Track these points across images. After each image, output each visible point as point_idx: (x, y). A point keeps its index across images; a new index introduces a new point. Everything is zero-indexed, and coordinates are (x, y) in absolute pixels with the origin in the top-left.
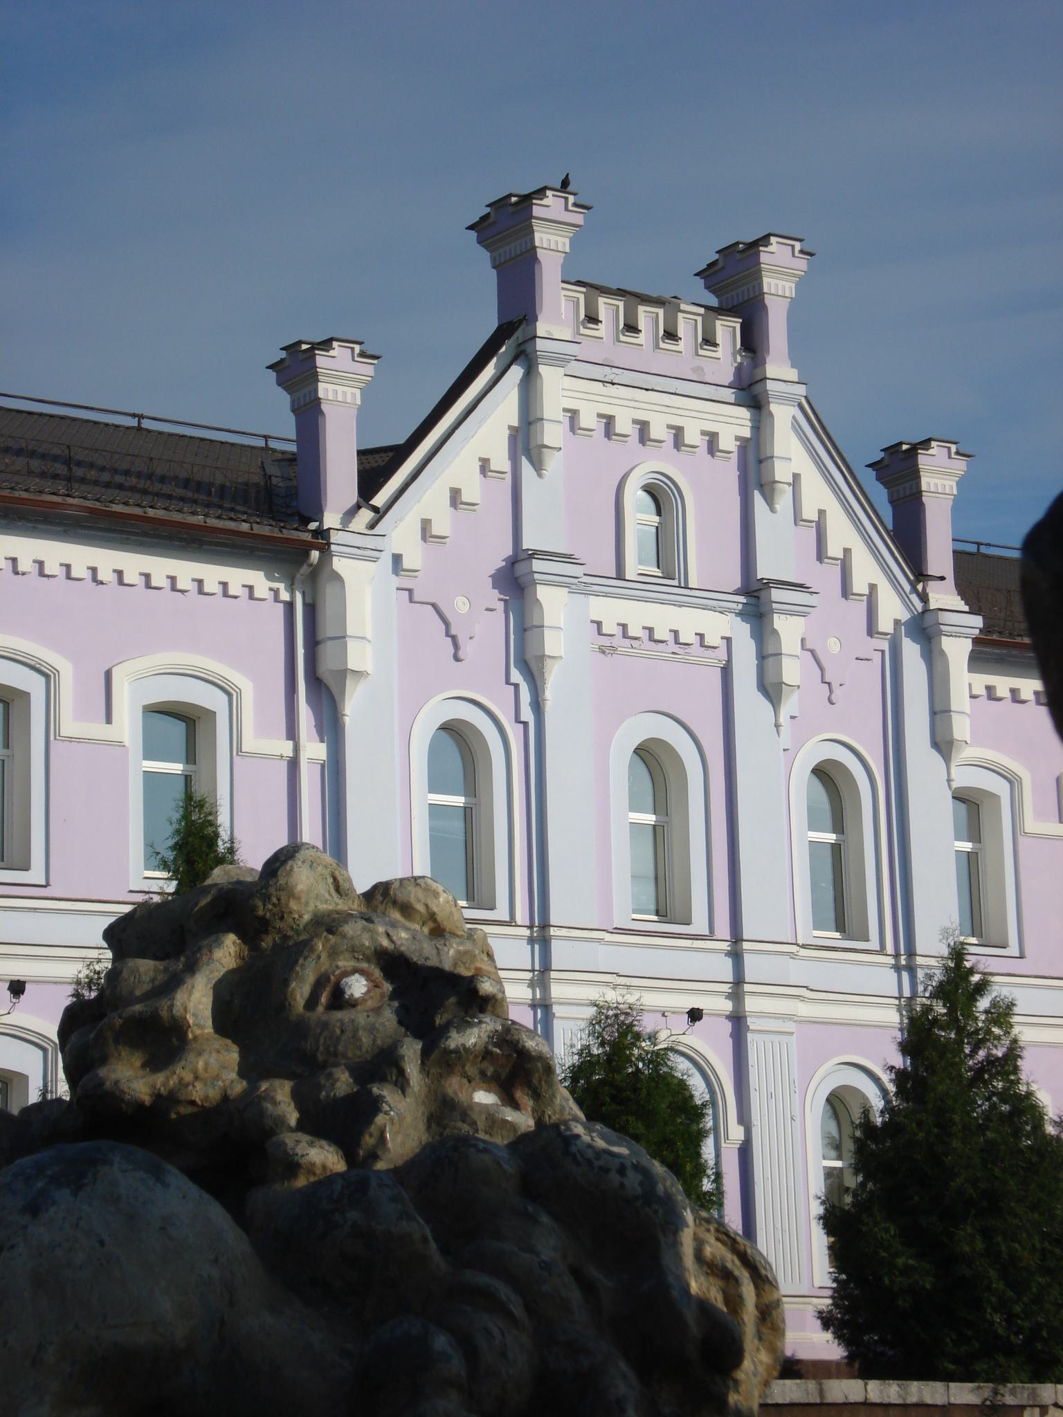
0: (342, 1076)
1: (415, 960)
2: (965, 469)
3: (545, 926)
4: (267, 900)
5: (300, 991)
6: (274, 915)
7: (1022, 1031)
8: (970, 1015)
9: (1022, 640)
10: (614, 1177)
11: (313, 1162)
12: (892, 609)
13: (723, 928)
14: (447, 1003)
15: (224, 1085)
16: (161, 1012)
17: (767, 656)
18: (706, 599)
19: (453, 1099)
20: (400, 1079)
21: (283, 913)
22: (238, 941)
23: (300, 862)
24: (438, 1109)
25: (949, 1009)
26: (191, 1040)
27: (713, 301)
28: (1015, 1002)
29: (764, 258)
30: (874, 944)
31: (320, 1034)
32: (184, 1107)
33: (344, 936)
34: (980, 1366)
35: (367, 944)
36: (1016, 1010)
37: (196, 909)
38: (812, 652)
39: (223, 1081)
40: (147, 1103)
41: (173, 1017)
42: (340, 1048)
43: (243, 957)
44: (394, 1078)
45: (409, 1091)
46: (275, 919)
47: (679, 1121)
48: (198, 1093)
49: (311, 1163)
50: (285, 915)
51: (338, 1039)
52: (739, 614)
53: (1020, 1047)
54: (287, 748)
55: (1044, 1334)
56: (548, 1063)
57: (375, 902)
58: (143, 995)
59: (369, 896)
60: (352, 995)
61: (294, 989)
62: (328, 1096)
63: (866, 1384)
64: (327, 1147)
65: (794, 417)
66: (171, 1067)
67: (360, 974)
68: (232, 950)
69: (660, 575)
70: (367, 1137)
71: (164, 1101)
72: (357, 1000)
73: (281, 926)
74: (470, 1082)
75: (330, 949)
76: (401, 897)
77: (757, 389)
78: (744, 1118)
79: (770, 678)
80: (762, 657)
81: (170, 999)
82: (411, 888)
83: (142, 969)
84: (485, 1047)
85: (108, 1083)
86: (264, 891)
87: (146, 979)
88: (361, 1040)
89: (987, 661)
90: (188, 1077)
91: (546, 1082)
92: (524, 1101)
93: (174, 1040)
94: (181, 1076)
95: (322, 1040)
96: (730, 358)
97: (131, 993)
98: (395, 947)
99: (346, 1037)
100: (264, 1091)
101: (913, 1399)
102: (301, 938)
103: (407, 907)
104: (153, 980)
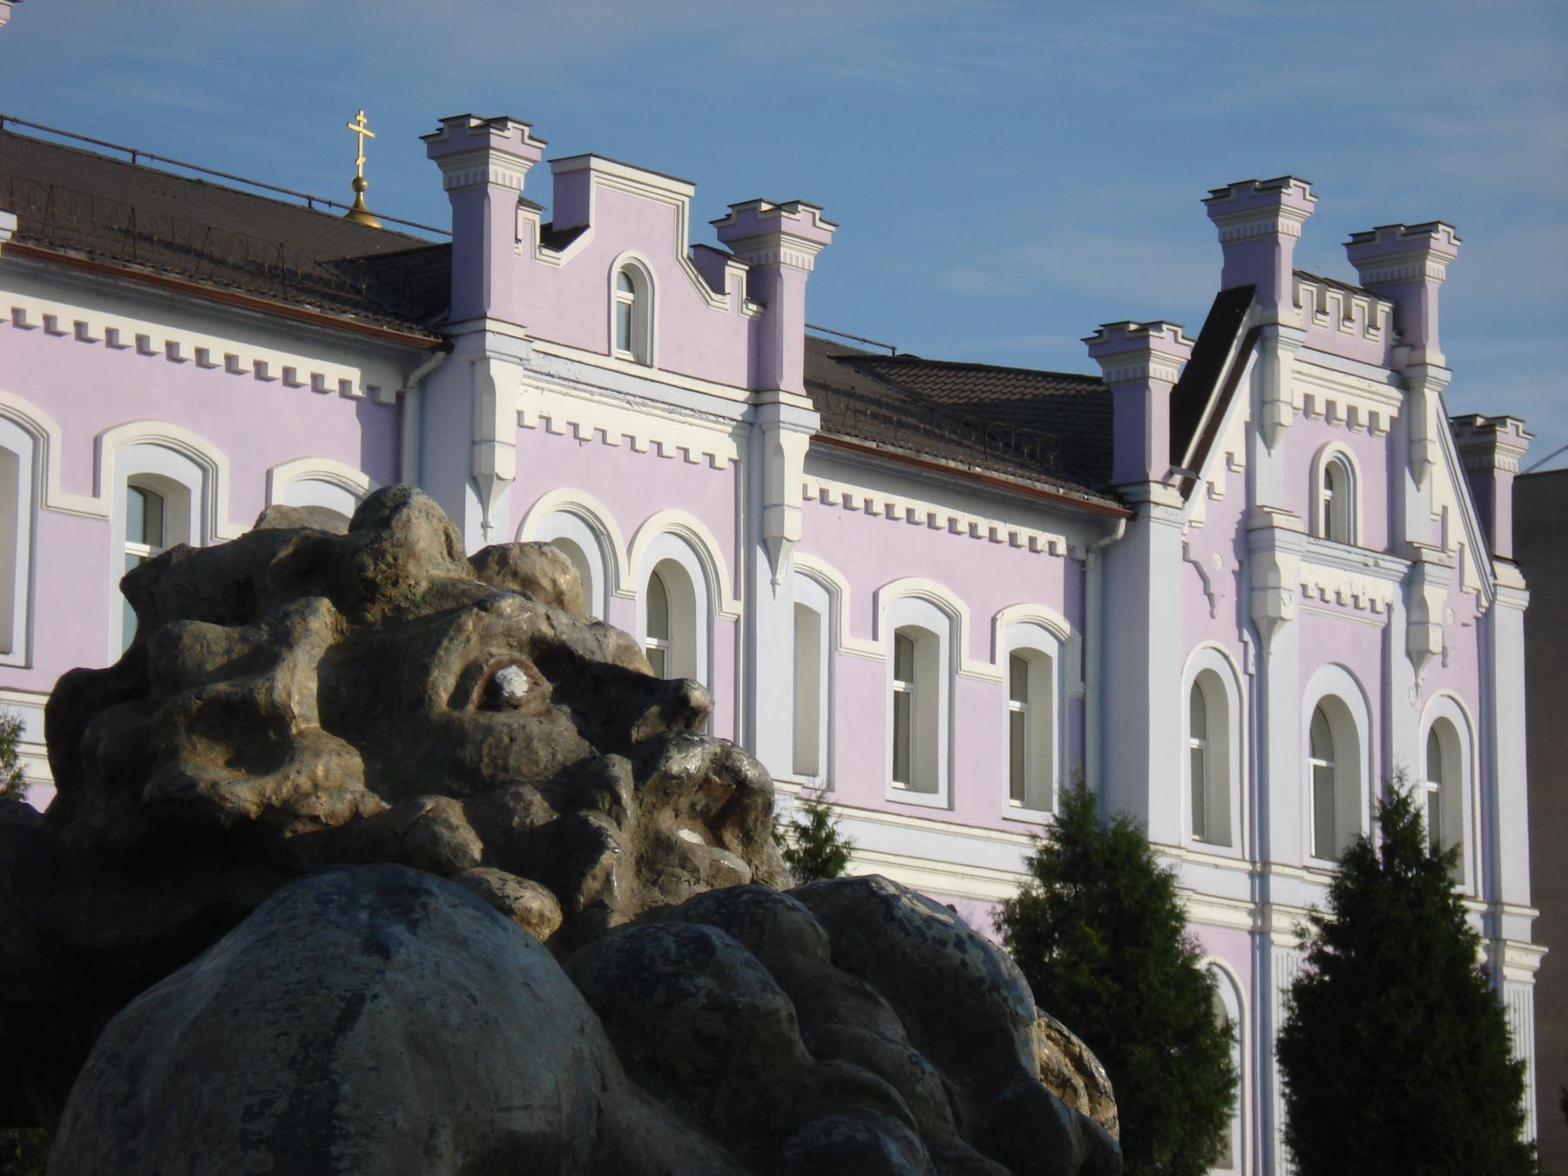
0: (534, 798)
1: (581, 653)
2: (8, 17)
3: (1266, 863)
4: (380, 558)
5: (444, 684)
6: (387, 578)
7: (29, 764)
9: (65, 252)
10: (951, 949)
11: (529, 907)
14: (648, 713)
15: (355, 799)
16: (257, 695)
19: (669, 838)
20: (615, 807)
21: (398, 576)
22: (333, 609)
23: (416, 512)
24: (649, 849)
26: (294, 736)
28: (23, 726)
31: (482, 741)
32: (304, 824)
33: (500, 615)
35: (525, 628)
36: (24, 736)
37: (274, 562)
38: (1196, 564)
40: (253, 816)
41: (273, 704)
42: (511, 762)
43: (342, 629)
44: (607, 806)
45: (625, 823)
46: (386, 585)
48: (323, 806)
49: (526, 909)
50: (400, 580)
51: (507, 749)
53: (24, 784)
54: (1386, 403)
55: (18, 1152)
56: (769, 799)
57: (489, 572)
58: (216, 670)
59: (481, 560)
60: (513, 693)
61: (436, 679)
62: (523, 823)
64: (540, 890)
66: (282, 769)
67: (518, 667)
68: (329, 619)
70: (589, 878)
71: (277, 814)
72: (519, 699)
73: (393, 594)
74: (677, 816)
75: (483, 630)
76: (524, 568)
81: (268, 680)
82: (535, 557)
83: (209, 636)
84: (706, 774)
85: (202, 785)
86: (376, 545)
87: (218, 648)
88: (537, 753)
90: (305, 783)
91: (762, 822)
92: (734, 845)
93: (271, 733)
94: (297, 782)
95: (485, 750)
97: (200, 666)
98: (555, 635)
99: (517, 747)
100: (430, 810)
103: (531, 581)
104: (228, 652)
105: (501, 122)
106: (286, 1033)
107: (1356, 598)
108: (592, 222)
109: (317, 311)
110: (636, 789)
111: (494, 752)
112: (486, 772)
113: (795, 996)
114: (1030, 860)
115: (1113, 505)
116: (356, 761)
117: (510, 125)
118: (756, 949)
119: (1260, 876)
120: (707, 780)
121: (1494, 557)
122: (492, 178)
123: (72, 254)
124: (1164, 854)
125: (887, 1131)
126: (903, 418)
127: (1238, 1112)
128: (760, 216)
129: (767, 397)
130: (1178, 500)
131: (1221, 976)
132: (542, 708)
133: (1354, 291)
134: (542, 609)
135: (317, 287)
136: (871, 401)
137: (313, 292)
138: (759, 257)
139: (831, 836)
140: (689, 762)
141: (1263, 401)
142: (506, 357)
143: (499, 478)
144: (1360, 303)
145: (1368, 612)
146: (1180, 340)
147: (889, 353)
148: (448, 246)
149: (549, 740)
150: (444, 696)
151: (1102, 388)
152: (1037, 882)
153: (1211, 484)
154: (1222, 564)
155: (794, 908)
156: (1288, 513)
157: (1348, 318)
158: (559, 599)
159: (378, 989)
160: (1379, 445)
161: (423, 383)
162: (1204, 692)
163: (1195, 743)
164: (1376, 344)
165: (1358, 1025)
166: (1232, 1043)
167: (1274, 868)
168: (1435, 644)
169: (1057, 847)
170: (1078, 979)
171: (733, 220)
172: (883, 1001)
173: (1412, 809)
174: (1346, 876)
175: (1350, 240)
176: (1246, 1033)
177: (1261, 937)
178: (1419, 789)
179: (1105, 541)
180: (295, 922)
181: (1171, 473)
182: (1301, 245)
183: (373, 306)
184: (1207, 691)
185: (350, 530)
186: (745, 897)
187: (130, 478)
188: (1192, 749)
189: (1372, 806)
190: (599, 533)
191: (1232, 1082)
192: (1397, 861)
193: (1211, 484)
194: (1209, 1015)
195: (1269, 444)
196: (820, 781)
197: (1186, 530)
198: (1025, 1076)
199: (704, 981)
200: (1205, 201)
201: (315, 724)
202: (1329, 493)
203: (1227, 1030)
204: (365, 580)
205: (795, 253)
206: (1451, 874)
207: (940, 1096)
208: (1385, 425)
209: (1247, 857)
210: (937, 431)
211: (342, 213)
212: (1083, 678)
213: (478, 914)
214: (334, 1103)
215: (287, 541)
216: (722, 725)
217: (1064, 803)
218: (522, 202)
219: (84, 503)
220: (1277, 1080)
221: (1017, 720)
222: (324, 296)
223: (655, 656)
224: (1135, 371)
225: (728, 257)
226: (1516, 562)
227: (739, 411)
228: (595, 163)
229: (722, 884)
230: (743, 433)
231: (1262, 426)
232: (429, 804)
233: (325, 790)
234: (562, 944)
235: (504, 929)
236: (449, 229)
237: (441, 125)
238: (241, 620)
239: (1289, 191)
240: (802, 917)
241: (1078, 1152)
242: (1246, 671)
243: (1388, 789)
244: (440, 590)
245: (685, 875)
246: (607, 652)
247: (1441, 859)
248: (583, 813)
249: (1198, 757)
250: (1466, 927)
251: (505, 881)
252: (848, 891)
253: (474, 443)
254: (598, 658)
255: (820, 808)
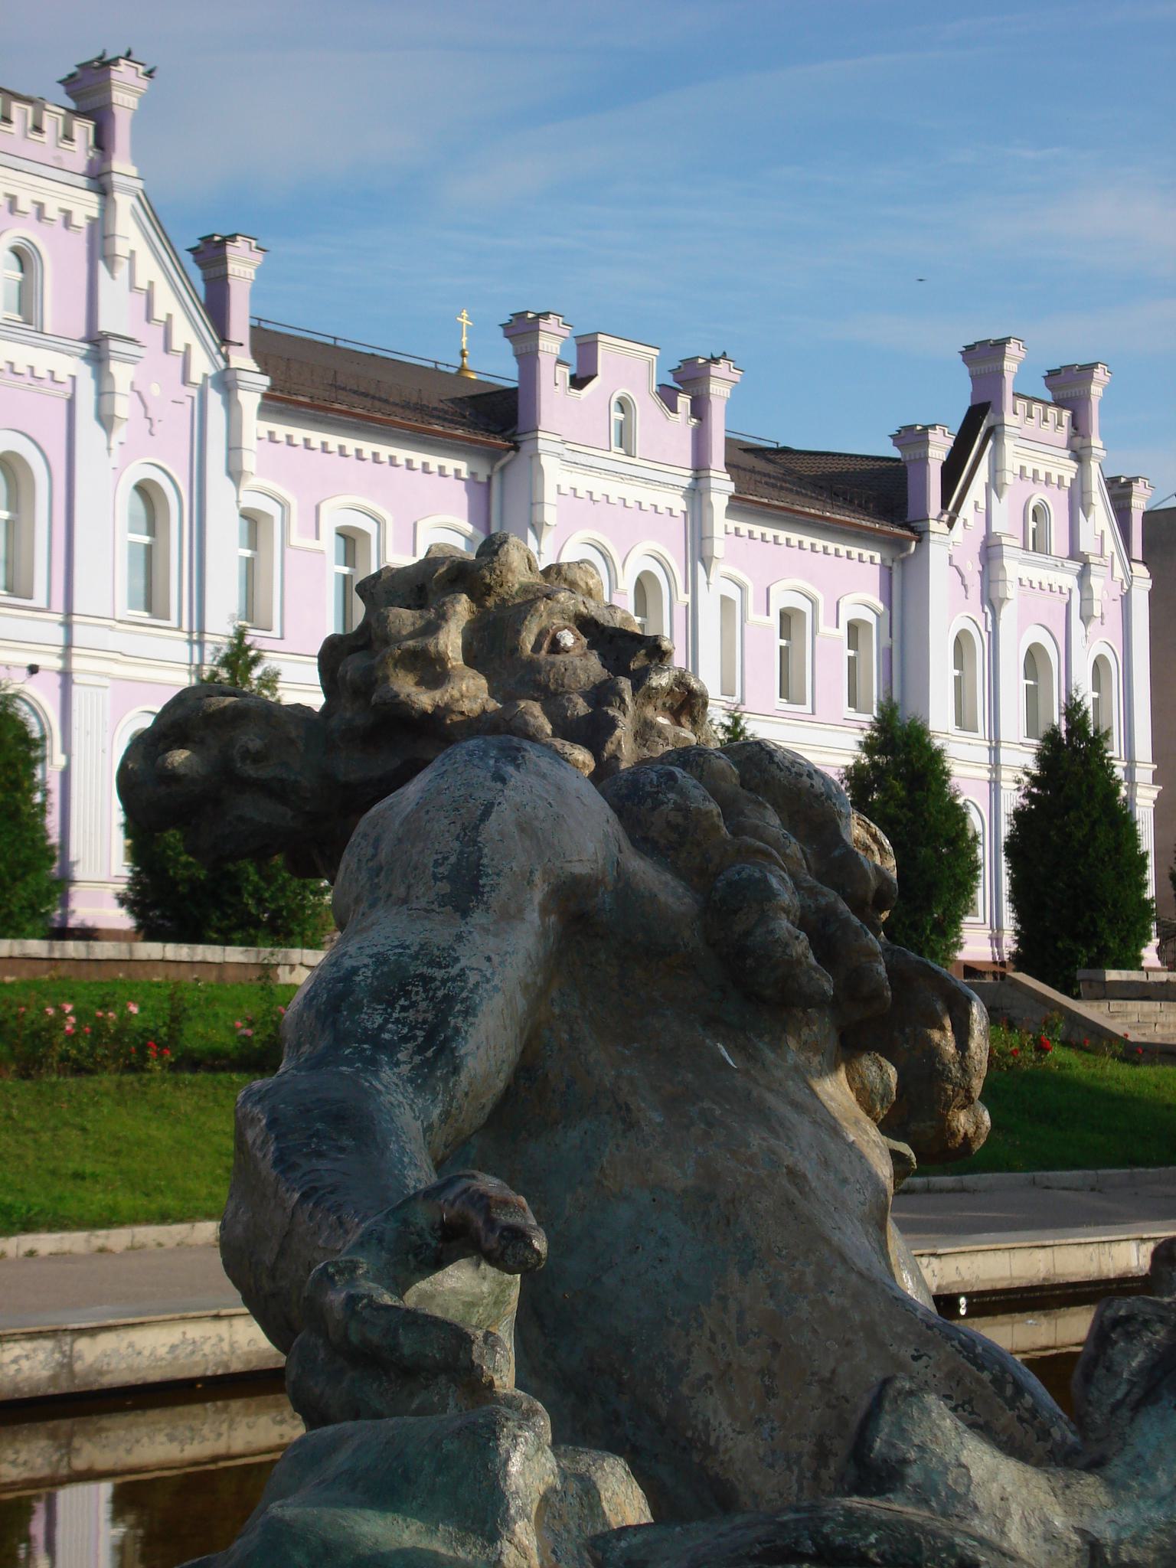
3: (998, 741)
5: (528, 640)
8: (247, 681)
10: (805, 778)
12: (202, 365)
13: (58, 604)
17: (104, 393)
18: (57, 343)
25: (231, 674)
27: (72, 106)
29: (114, 75)
30: (174, 623)
31: (550, 671)
33: (558, 602)
34: (237, 935)
36: (281, 678)
38: (139, 393)
39: (482, 699)
40: (430, 712)
41: (438, 652)
42: (566, 681)
47: (20, 749)
48: (466, 706)
52: (84, 358)
54: (1068, 470)
59: (546, 573)
60: (566, 644)
62: (573, 714)
63: (164, 947)
65: (133, 206)
69: (21, 320)
70: (609, 743)
71: (442, 711)
72: (569, 648)
76: (570, 576)
77: (105, 179)
78: (66, 749)
79: (106, 411)
80: (100, 394)
85: (402, 695)
89: (270, 412)
90: (456, 694)
95: (551, 676)
96: (83, 152)
101: (198, 958)
102: (517, 601)
104: (413, 624)
105: (546, 315)
106: (454, 823)
107: (1050, 585)
108: (600, 371)
109: (440, 429)
110: (633, 695)
111: (556, 676)
112: (552, 687)
113: (721, 804)
114: (860, 742)
115: (908, 533)
116: (483, 682)
117: (551, 316)
118: (700, 779)
119: (995, 749)
120: (672, 690)
121: (1131, 560)
122: (541, 348)
123: (301, 399)
124: (938, 737)
125: (771, 872)
126: (784, 485)
127: (982, 885)
128: (698, 367)
129: (703, 473)
130: (946, 529)
131: (972, 807)
132: (582, 652)
133: (1049, 404)
134: (580, 598)
135: (441, 414)
136: (765, 475)
137: (439, 418)
138: (698, 392)
139: (743, 731)
140: (661, 680)
141: (996, 470)
142: (548, 452)
143: (548, 525)
144: (1052, 411)
145: (48, 383)
146: (947, 435)
147: (775, 446)
148: (515, 390)
149: (586, 670)
150: (529, 647)
151: (901, 464)
152: (864, 755)
153: (965, 520)
154: (972, 567)
155: (720, 757)
156: (1011, 536)
157: (1046, 420)
158: (589, 593)
159: (501, 799)
160: (1064, 495)
161: (503, 469)
162: (962, 644)
163: (957, 672)
164: (1063, 434)
165: (1052, 833)
166: (978, 845)
167: (1002, 744)
168: (1097, 612)
169: (876, 734)
170: (888, 810)
171: (682, 370)
172: (768, 805)
173: (1083, 708)
174: (1045, 747)
175: (1047, 374)
176: (986, 839)
177: (995, 785)
178: (1087, 696)
179: (904, 555)
180: (456, 765)
181: (942, 514)
182: (1017, 376)
183: (473, 426)
184: (964, 642)
185: (478, 556)
186: (693, 752)
187: (337, 529)
188: (955, 677)
189: (1060, 707)
190: (605, 556)
191: (978, 868)
192: (1074, 738)
193: (965, 520)
194: (964, 830)
195: (999, 495)
196: (737, 699)
197: (951, 547)
198: (845, 845)
199: (671, 796)
200: (961, 352)
201: (461, 662)
202: (1035, 524)
203: (975, 838)
204: (485, 584)
205: (719, 388)
206: (1106, 745)
207: (800, 855)
208: (1067, 483)
209: (987, 738)
210: (803, 491)
211: (453, 371)
212: (891, 636)
213: (551, 761)
214: (480, 858)
215: (443, 563)
216: (679, 660)
217: (880, 709)
218: (559, 362)
219: (311, 543)
220: (1004, 866)
221: (852, 661)
222: (445, 419)
223: (642, 626)
224: (920, 454)
225: (679, 391)
226: (1144, 563)
227: (687, 482)
228: (601, 337)
229: (680, 746)
230: (690, 495)
231: (995, 485)
232: (523, 704)
233: (467, 697)
234: (596, 778)
235: (565, 768)
236: (516, 379)
237: (511, 318)
238: (420, 607)
239: (1010, 346)
240: (724, 762)
241: (874, 883)
242: (986, 630)
243: (1069, 697)
244: (525, 589)
245: (661, 741)
246: (616, 622)
247: (1100, 737)
248: (605, 708)
249: (958, 680)
250: (1114, 776)
251: (564, 745)
252: (749, 748)
253: (532, 504)
254: (612, 625)
255: (737, 714)
